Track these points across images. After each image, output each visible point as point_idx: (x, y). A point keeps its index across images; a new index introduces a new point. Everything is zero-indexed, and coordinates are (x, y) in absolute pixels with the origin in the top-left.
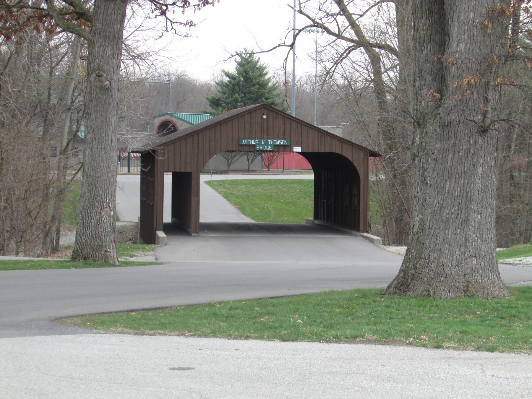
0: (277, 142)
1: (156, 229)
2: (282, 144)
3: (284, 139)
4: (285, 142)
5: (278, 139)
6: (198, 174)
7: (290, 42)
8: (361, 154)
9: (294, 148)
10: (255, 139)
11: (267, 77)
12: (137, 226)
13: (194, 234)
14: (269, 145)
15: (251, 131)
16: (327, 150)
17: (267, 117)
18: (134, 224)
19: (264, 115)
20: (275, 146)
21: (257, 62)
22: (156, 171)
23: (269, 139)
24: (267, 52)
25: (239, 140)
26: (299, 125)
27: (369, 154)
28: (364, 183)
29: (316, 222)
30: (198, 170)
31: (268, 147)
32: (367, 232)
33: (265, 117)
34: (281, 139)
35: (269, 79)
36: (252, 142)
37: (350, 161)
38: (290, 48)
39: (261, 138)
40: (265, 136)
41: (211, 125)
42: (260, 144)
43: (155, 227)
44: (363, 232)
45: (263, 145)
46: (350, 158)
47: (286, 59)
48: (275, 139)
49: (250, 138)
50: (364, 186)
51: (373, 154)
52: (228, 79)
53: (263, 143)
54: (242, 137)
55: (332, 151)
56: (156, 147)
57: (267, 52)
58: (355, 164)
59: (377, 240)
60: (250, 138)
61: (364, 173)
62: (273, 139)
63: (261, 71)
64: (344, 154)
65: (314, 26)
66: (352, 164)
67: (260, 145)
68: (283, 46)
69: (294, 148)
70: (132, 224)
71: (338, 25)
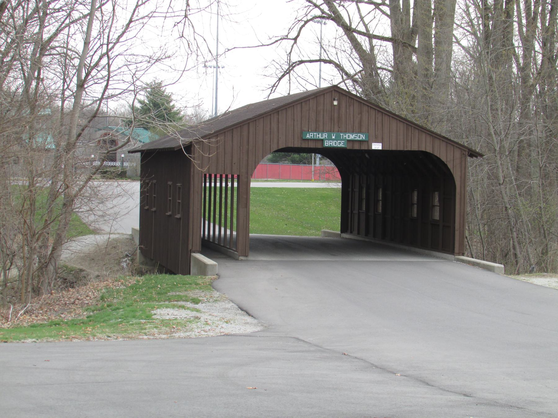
0: (352, 137)
1: (191, 251)
2: (357, 138)
3: (360, 132)
4: (362, 137)
5: (353, 132)
6: (247, 178)
7: (293, 35)
8: (458, 153)
9: (373, 144)
10: (323, 132)
11: (171, 104)
12: (132, 238)
13: (241, 258)
14: (341, 140)
15: (317, 121)
16: (415, 148)
17: (339, 103)
18: (128, 237)
19: (334, 100)
20: (349, 141)
21: (164, 92)
22: (192, 174)
23: (341, 132)
24: (268, 45)
25: (302, 133)
26: (380, 114)
27: (467, 153)
28: (461, 192)
29: (345, 236)
30: (247, 173)
31: (340, 143)
32: (463, 255)
33: (335, 103)
34: (356, 133)
35: (173, 105)
36: (319, 136)
37: (443, 162)
38: (293, 41)
39: (330, 131)
40: (336, 129)
41: (265, 113)
42: (330, 139)
43: (190, 247)
44: (459, 254)
45: (333, 140)
46: (443, 159)
47: (290, 53)
48: (349, 132)
49: (316, 131)
50: (461, 196)
51: (473, 154)
52: (141, 105)
53: (333, 137)
54: (306, 129)
55: (420, 149)
56: (202, 137)
57: (268, 45)
58: (450, 166)
59: (499, 267)
60: (316, 130)
61: (461, 177)
62: (346, 132)
63: (168, 99)
64: (436, 154)
65: (323, 17)
66: (446, 166)
67: (329, 140)
68: (285, 39)
69: (373, 144)
70: (125, 236)
71: (349, 16)
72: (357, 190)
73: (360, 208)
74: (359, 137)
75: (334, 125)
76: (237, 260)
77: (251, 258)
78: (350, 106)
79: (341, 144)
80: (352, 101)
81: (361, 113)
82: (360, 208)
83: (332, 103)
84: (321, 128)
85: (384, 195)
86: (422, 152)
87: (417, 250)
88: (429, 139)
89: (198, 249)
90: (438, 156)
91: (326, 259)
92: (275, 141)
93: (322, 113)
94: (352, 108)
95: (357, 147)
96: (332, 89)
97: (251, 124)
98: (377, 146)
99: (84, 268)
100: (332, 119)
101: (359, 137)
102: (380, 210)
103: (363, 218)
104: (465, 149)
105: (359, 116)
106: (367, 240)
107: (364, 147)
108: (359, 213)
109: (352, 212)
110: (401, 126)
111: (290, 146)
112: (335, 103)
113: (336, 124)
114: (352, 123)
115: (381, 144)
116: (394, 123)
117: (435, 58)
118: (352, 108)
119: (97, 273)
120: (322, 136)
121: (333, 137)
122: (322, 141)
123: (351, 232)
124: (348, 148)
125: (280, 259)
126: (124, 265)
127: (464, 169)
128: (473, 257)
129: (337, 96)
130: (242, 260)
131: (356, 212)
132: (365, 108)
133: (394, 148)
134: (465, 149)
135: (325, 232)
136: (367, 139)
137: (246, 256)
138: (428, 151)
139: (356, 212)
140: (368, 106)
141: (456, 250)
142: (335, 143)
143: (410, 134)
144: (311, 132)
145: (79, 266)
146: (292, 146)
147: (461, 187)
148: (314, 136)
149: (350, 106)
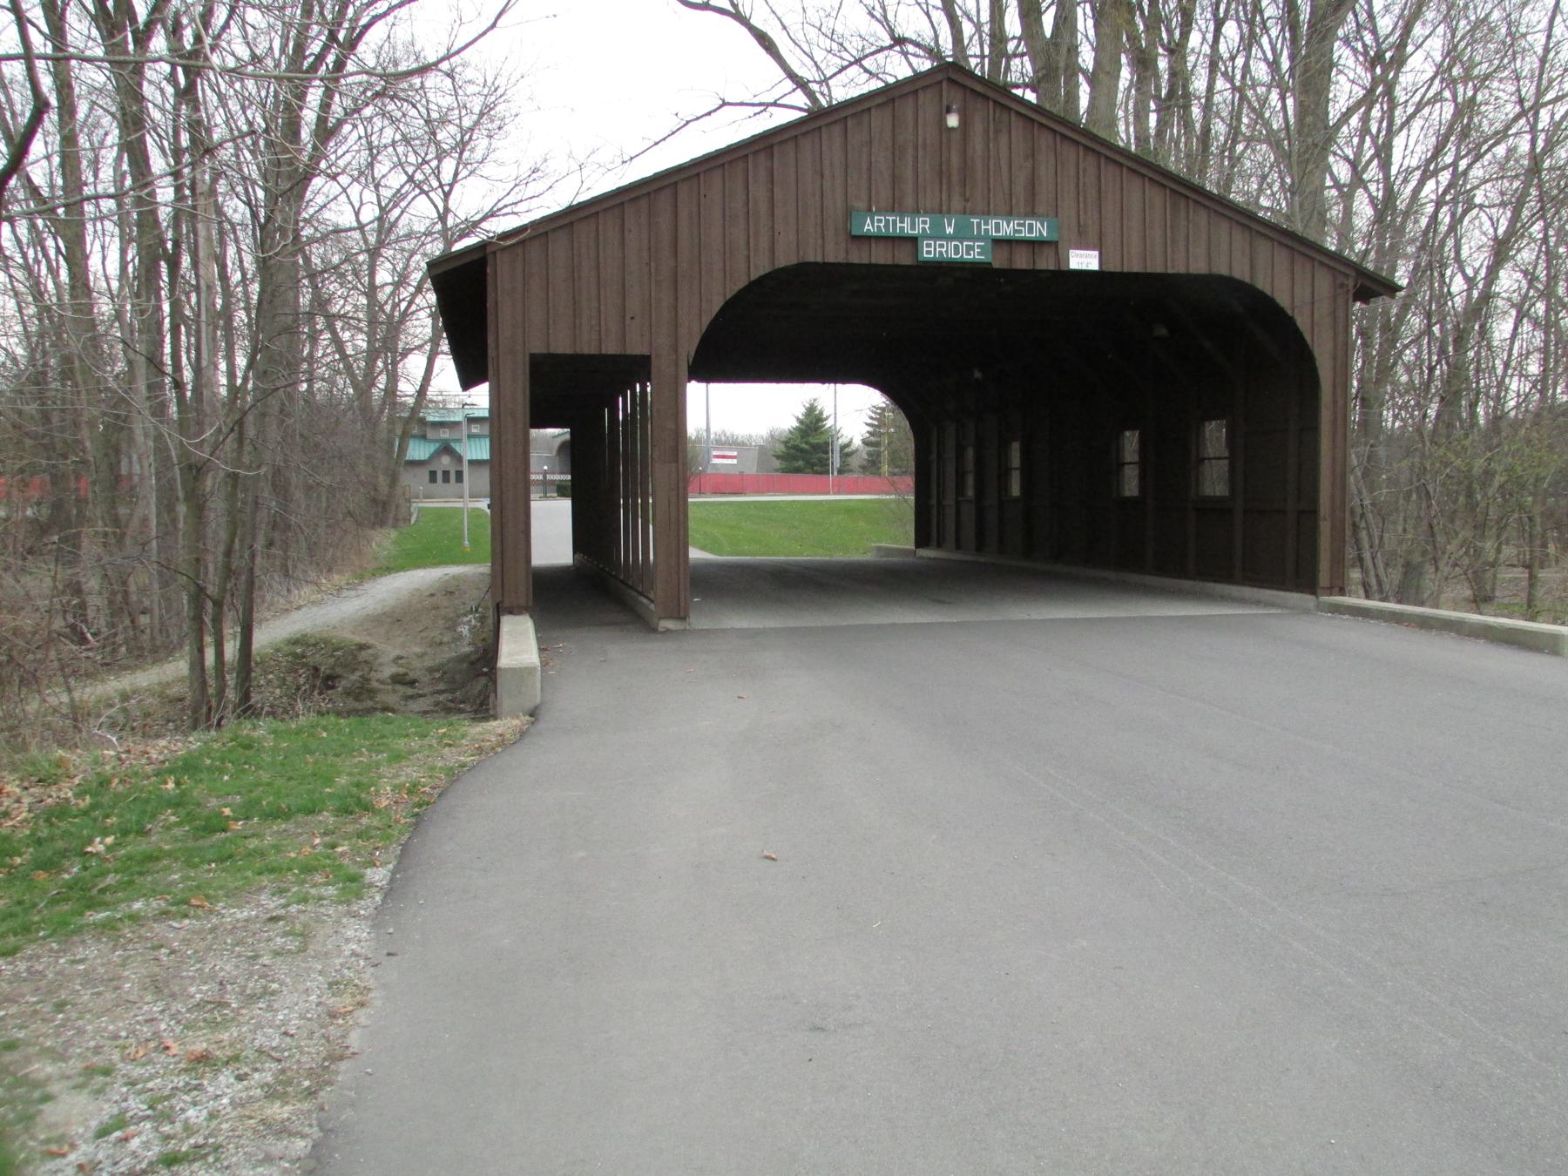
0: (1008, 229)
2: (1025, 234)
3: (1032, 213)
4: (1038, 229)
5: (1009, 214)
8: (1324, 283)
10: (916, 211)
14: (978, 238)
15: (895, 179)
16: (1199, 267)
17: (964, 121)
19: (949, 111)
20: (997, 242)
23: (974, 214)
25: (848, 213)
26: (1091, 159)
27: (1351, 283)
28: (1335, 402)
31: (970, 248)
33: (953, 121)
34: (1019, 216)
36: (906, 226)
39: (940, 210)
40: (957, 202)
44: (1330, 590)
45: (950, 238)
46: (1283, 300)
48: (996, 215)
53: (950, 230)
54: (862, 205)
58: (1302, 322)
60: (895, 207)
61: (1335, 358)
62: (987, 213)
64: (1262, 284)
72: (950, 454)
73: (960, 489)
74: (1031, 231)
75: (949, 183)
76: (654, 630)
77: (698, 621)
78: (997, 131)
79: (974, 253)
80: (1005, 116)
81: (1032, 155)
82: (960, 489)
83: (942, 121)
84: (909, 201)
85: (1025, 453)
86: (1221, 278)
87: (1149, 580)
88: (1240, 238)
89: (522, 602)
90: (1268, 291)
91: (940, 620)
92: (764, 242)
93: (910, 151)
94: (1004, 139)
95: (1022, 262)
96: (940, 77)
97: (683, 190)
98: (1084, 260)
99: (371, 641)
100: (941, 173)
101: (1031, 231)
102: (1016, 491)
103: (969, 513)
104: (1348, 271)
105: (1029, 164)
106: (982, 560)
107: (1046, 263)
108: (958, 503)
109: (939, 502)
110: (1156, 197)
111: (811, 259)
112: (953, 121)
113: (960, 189)
114: (1006, 183)
115: (1096, 253)
116: (1134, 188)
117: (1158, 111)
118: (1004, 139)
119: (398, 652)
120: (913, 227)
121: (950, 230)
122: (914, 241)
123: (939, 546)
124: (996, 265)
125: (792, 622)
126: (464, 630)
127: (1341, 325)
128: (1367, 597)
129: (953, 96)
130: (668, 631)
131: (950, 500)
132: (1045, 140)
133: (1135, 267)
134: (1348, 271)
135: (879, 549)
136: (1054, 237)
137: (682, 617)
138: (1237, 275)
139: (950, 500)
140: (1054, 131)
141: (1324, 578)
142: (956, 247)
143: (1183, 223)
144: (879, 212)
145: (358, 639)
146: (819, 259)
147: (1334, 386)
148: (887, 226)
149: (997, 131)
